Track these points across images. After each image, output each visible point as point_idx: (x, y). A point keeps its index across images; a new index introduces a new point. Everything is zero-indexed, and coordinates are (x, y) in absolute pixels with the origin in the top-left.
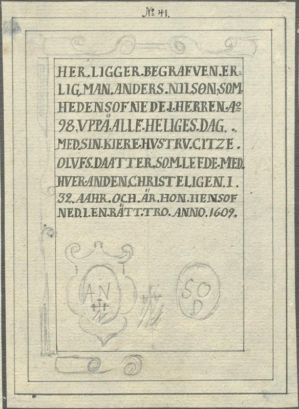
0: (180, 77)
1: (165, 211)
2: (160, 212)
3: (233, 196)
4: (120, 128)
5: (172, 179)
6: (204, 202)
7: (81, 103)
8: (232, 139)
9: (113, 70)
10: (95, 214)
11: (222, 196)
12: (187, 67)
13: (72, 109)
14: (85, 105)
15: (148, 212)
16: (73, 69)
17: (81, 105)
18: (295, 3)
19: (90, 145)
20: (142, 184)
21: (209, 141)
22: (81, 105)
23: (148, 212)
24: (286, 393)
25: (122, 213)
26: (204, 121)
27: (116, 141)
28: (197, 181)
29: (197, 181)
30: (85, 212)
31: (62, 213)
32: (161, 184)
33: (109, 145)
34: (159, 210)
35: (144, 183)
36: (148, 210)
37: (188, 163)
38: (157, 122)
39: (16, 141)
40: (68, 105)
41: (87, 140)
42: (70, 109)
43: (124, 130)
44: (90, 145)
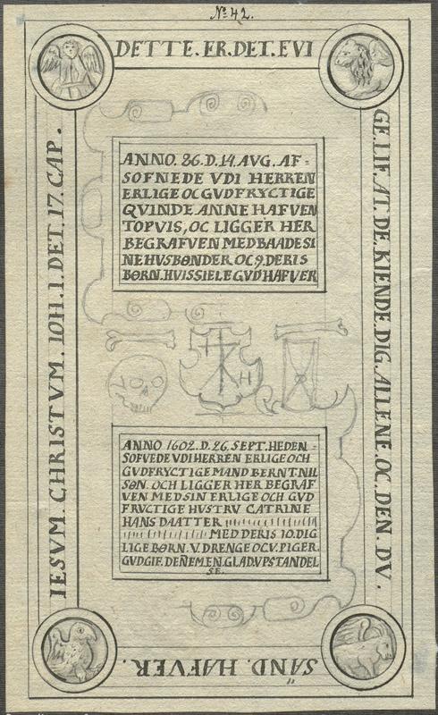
1: (170, 158)
2: (181, 259)
3: (197, 174)
4: (379, 385)
5: (173, 44)
6: (191, 214)
8: (389, 320)
9: (240, 225)
10: (379, 512)
11: (199, 273)
12: (388, 276)
15: (284, 192)
21: (386, 199)
22: (385, 224)
23: (284, 192)
24: (412, 696)
25: (180, 523)
26: (240, 44)
27: (386, 163)
28: (382, 352)
29: (382, 352)
30: (287, 508)
33: (379, 259)
34: (146, 272)
36: (184, 470)
37: (383, 407)
42: (379, 275)
43: (378, 404)
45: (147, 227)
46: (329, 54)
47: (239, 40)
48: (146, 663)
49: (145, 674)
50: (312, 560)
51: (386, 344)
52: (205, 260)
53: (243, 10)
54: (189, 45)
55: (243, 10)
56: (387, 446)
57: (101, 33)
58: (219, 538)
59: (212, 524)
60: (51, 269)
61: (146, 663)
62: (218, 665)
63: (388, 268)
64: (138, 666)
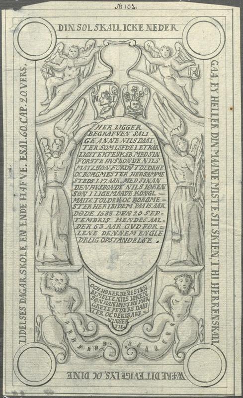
0: (210, 218)
7: (86, 379)
12: (218, 247)
13: (25, 79)
14: (164, 26)
16: (217, 248)
17: (87, 377)
18: (2, 10)
19: (216, 192)
20: (213, 99)
22: (87, 377)
27: (217, 245)
31: (215, 254)
32: (217, 232)
35: (213, 101)
38: (216, 104)
39: (29, 292)
40: (217, 290)
41: (218, 324)
44: (216, 192)
45: (23, 110)
46: (220, 348)
47: (87, 380)
48: (172, 30)
49: (172, 25)
50: (216, 107)
51: (217, 138)
52: (23, 212)
53: (133, 5)
54: (217, 293)
55: (133, 5)
56: (217, 178)
57: (216, 18)
58: (212, 156)
59: (213, 296)
60: (217, 132)
61: (172, 30)
62: (213, 72)
63: (218, 243)
64: (175, 29)
